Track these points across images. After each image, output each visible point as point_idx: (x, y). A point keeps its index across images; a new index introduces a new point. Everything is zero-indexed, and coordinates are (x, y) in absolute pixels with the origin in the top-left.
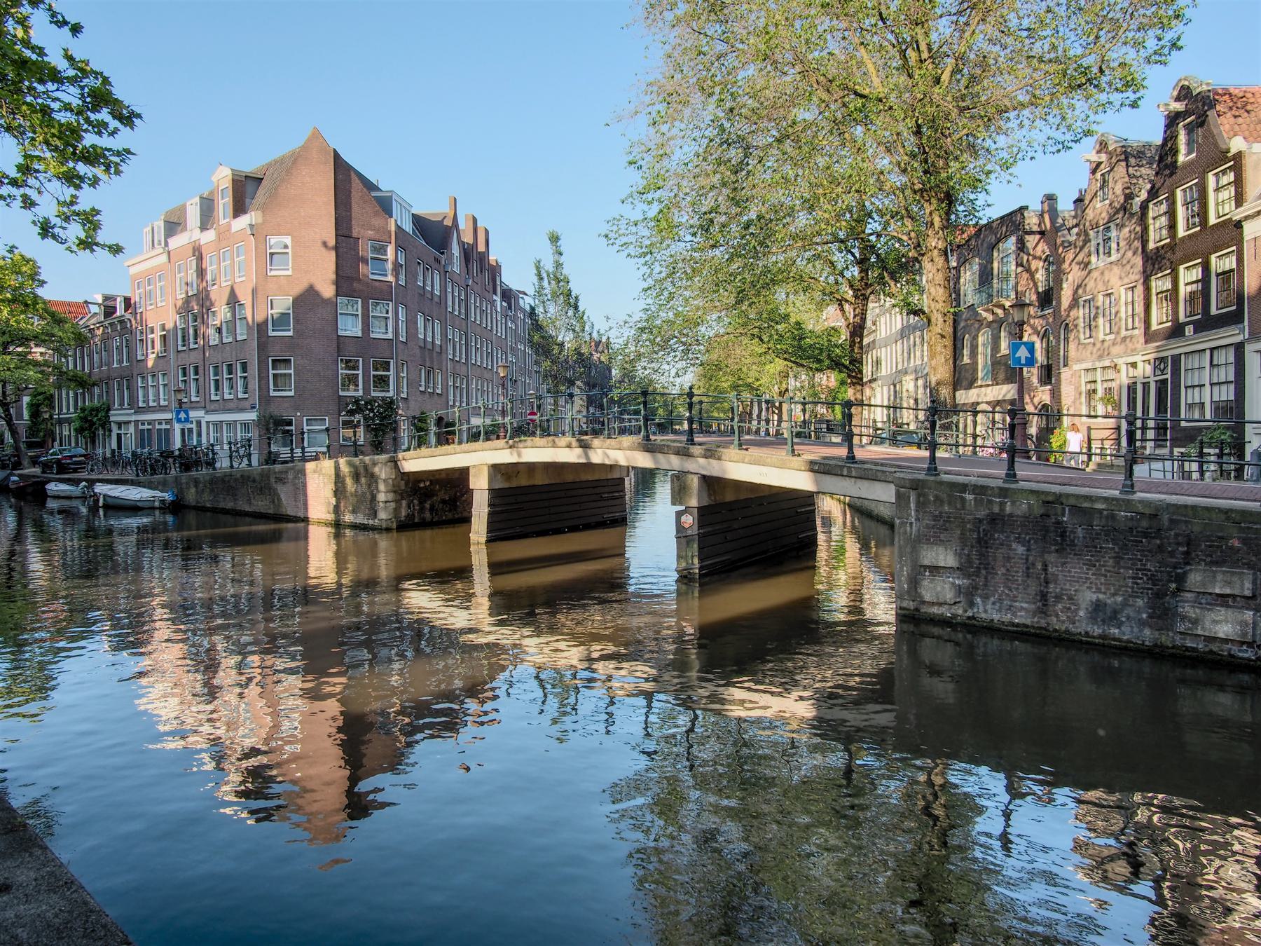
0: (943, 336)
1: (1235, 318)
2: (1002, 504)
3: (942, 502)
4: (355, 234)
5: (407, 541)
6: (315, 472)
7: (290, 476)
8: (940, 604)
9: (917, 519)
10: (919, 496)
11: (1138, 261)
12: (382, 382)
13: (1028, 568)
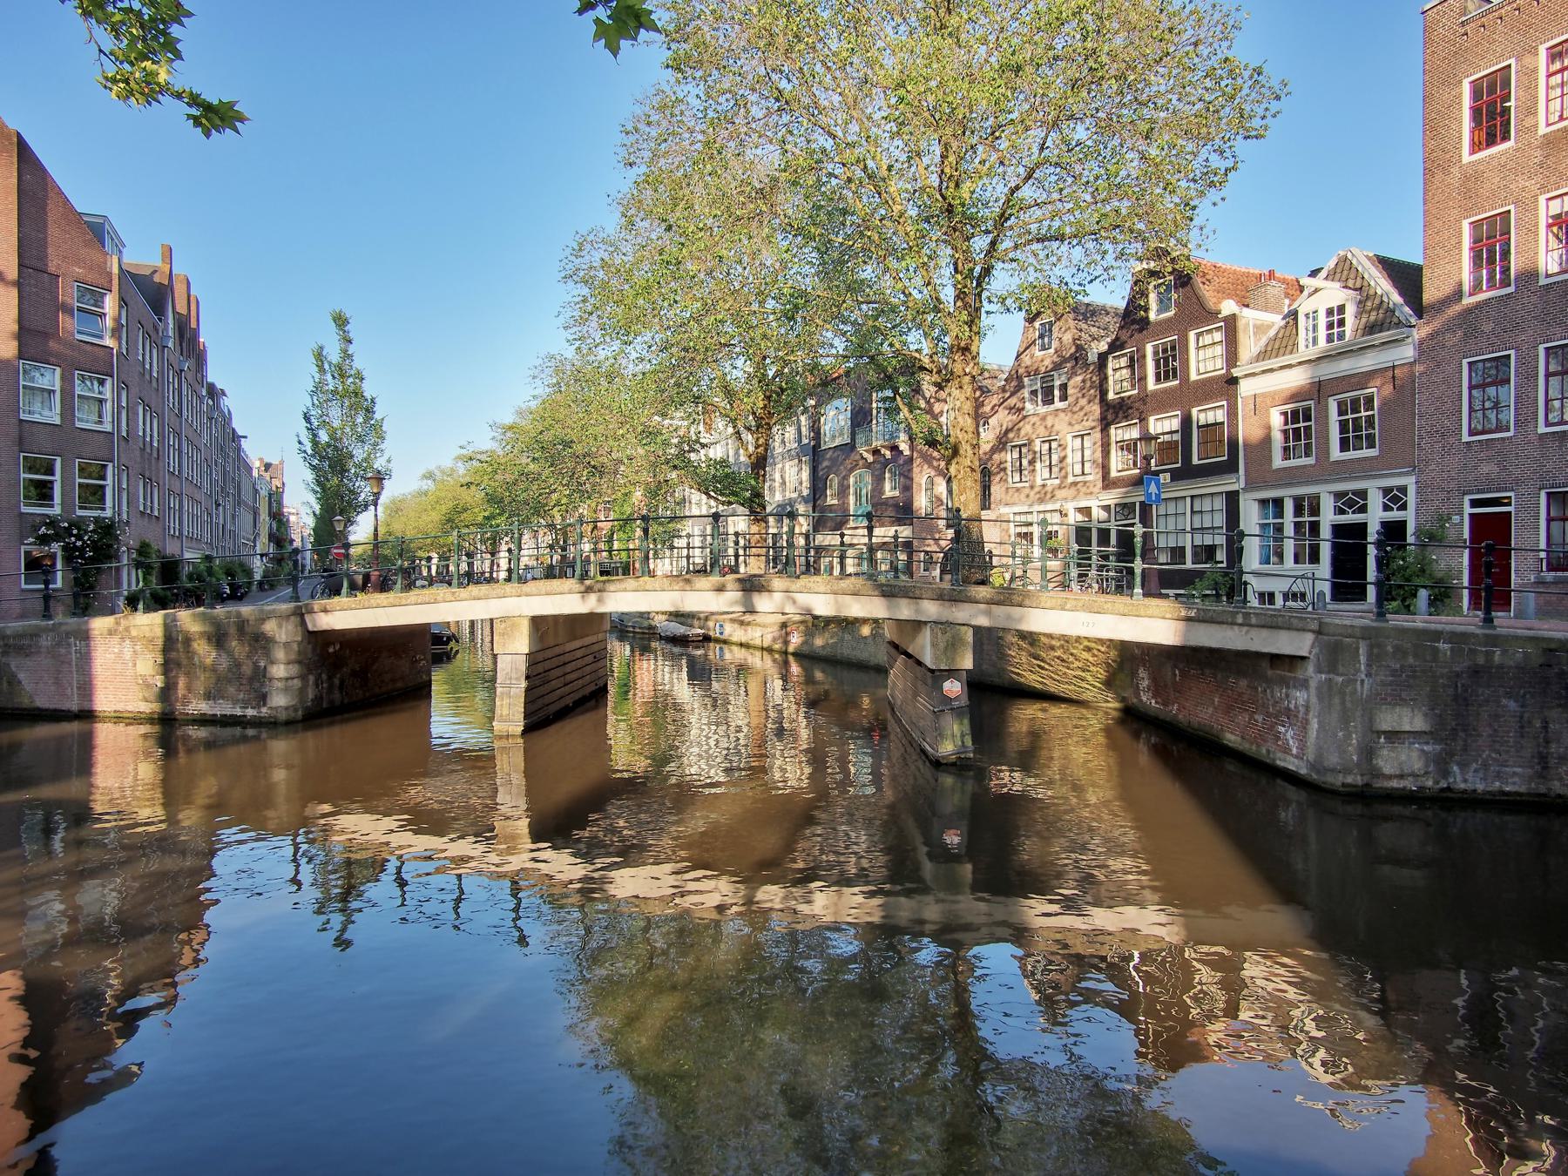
0: (973, 470)
1: (1230, 467)
2: (1489, 655)
3: (1405, 654)
4: (52, 269)
5: (314, 740)
6: (111, 633)
7: (45, 642)
8: (1401, 777)
9: (1369, 675)
10: (1371, 647)
11: (1096, 409)
12: (94, 495)
13: (1522, 727)
